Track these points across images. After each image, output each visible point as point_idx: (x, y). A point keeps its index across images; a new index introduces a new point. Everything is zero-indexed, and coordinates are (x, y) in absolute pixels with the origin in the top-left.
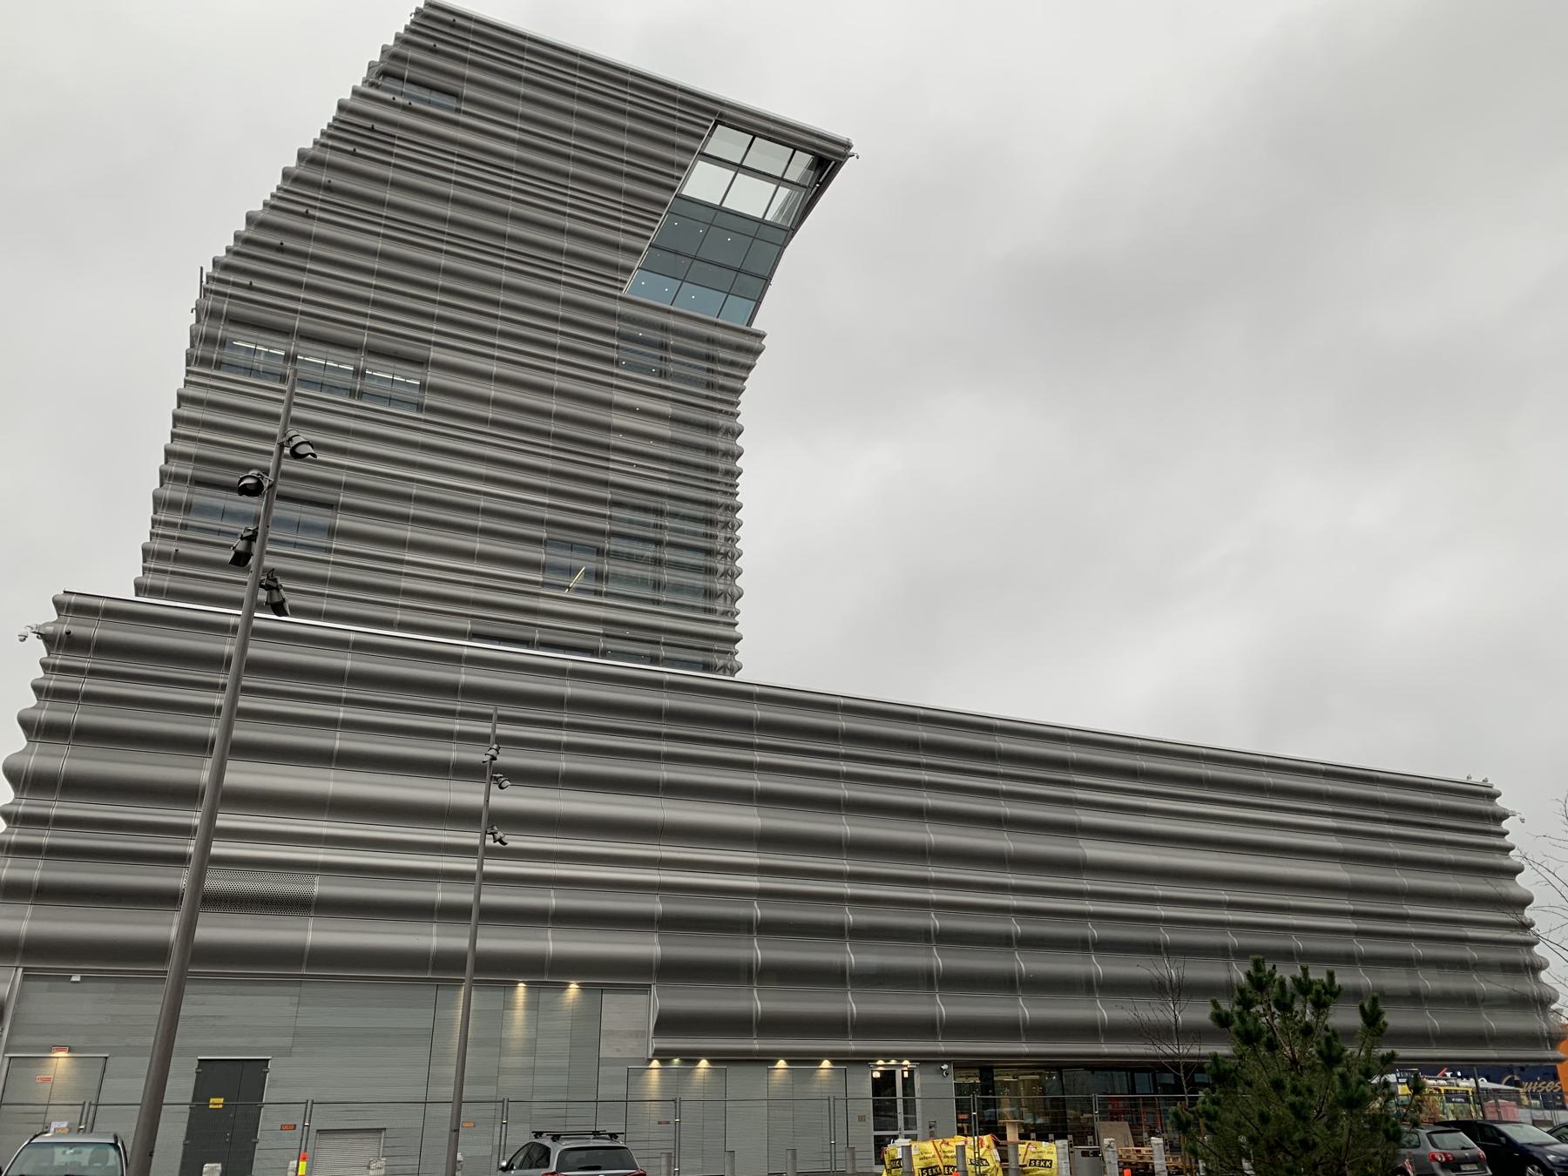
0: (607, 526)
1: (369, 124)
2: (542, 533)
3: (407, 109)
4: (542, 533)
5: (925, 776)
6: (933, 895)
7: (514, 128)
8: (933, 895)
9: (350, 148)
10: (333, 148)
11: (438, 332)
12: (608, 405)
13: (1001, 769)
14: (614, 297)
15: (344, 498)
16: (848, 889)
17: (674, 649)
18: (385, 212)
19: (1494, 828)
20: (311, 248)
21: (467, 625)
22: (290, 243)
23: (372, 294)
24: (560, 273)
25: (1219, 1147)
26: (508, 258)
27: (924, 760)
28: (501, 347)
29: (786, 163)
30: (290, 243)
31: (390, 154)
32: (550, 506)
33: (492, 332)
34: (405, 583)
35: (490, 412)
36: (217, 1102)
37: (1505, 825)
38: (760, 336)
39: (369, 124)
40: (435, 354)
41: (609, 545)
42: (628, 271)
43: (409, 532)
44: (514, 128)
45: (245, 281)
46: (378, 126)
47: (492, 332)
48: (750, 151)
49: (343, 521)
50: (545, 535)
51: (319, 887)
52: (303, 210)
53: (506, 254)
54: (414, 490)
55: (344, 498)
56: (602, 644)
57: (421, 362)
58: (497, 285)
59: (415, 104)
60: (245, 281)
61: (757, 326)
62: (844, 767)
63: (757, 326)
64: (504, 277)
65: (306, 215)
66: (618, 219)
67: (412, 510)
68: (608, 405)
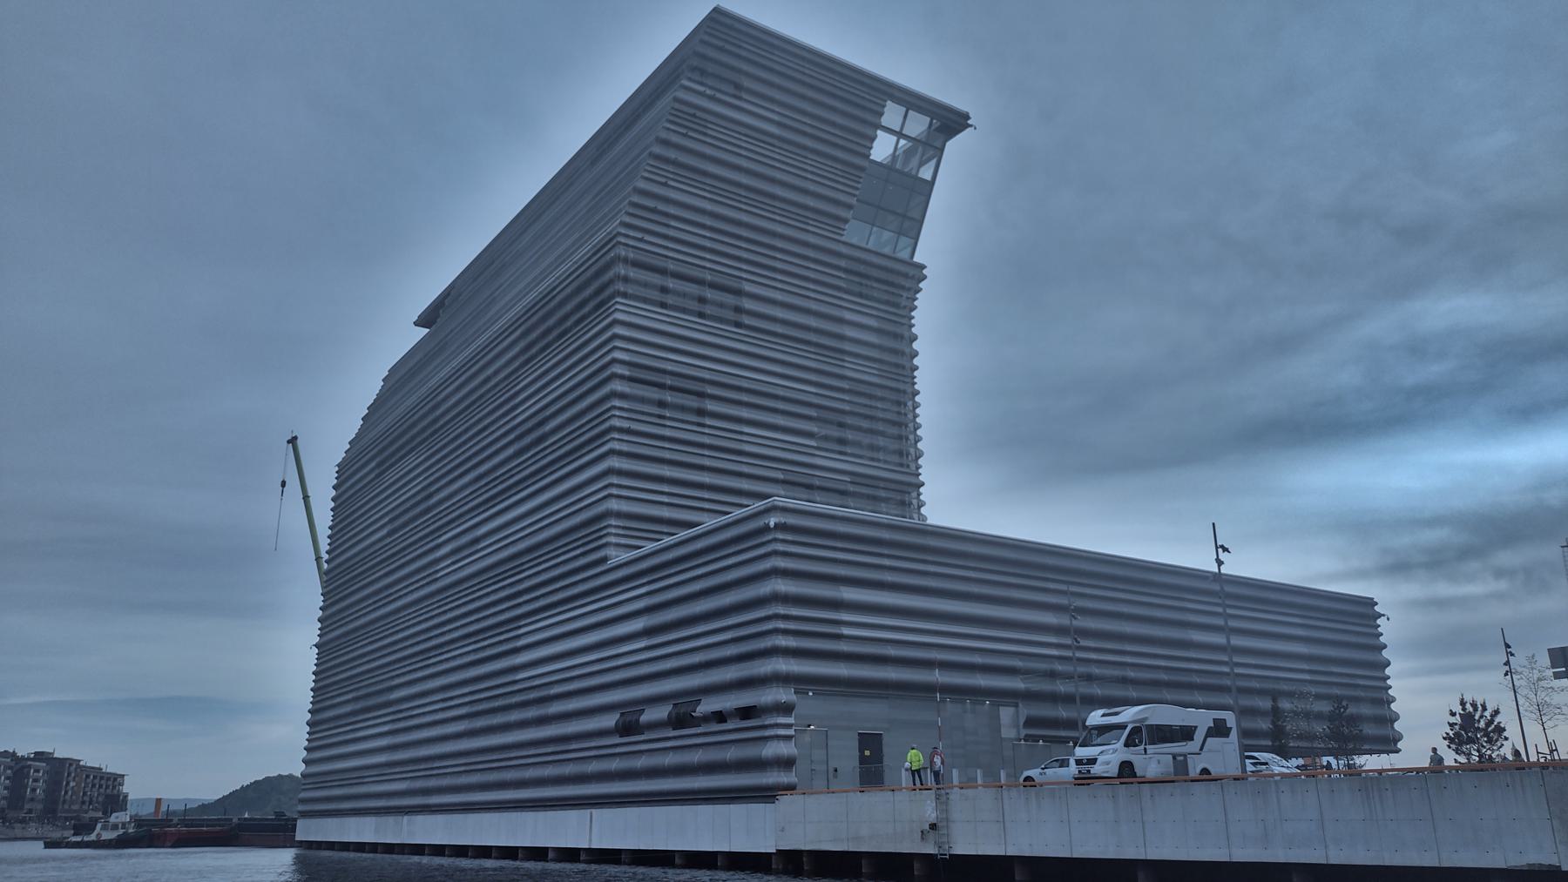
0: (847, 408)
1: (692, 111)
2: (813, 413)
3: (712, 98)
4: (813, 413)
5: (887, 562)
6: (1128, 659)
7: (773, 111)
8: (1128, 659)
9: (685, 131)
10: (674, 131)
11: (710, 261)
12: (841, 321)
13: (839, 545)
14: (839, 241)
15: (710, 390)
16: (1093, 656)
17: (651, 448)
18: (708, 181)
19: (1372, 623)
20: (672, 210)
21: (780, 476)
22: (661, 207)
23: (708, 244)
24: (808, 224)
25: (437, 870)
26: (780, 215)
27: (886, 552)
28: (781, 281)
29: (901, 119)
30: (661, 207)
31: (705, 134)
32: (816, 394)
33: (774, 269)
34: (747, 448)
35: (779, 329)
36: (867, 753)
37: (1379, 622)
38: (923, 267)
39: (692, 111)
40: (748, 287)
41: (849, 420)
42: (846, 221)
43: (745, 413)
44: (773, 111)
45: (639, 235)
46: (699, 114)
47: (774, 269)
48: (907, 122)
49: (711, 406)
50: (815, 414)
51: (892, 651)
52: (663, 180)
53: (743, 200)
54: (745, 384)
55: (710, 390)
56: (851, 488)
57: (738, 293)
58: (774, 234)
59: (719, 95)
60: (639, 235)
61: (916, 259)
62: (887, 562)
63: (916, 259)
64: (780, 229)
65: (665, 184)
66: (838, 182)
67: (745, 398)
68: (841, 321)
